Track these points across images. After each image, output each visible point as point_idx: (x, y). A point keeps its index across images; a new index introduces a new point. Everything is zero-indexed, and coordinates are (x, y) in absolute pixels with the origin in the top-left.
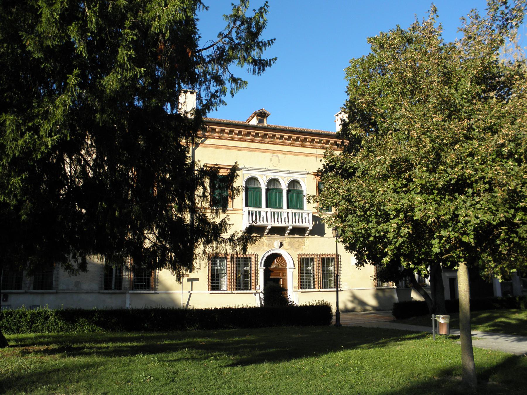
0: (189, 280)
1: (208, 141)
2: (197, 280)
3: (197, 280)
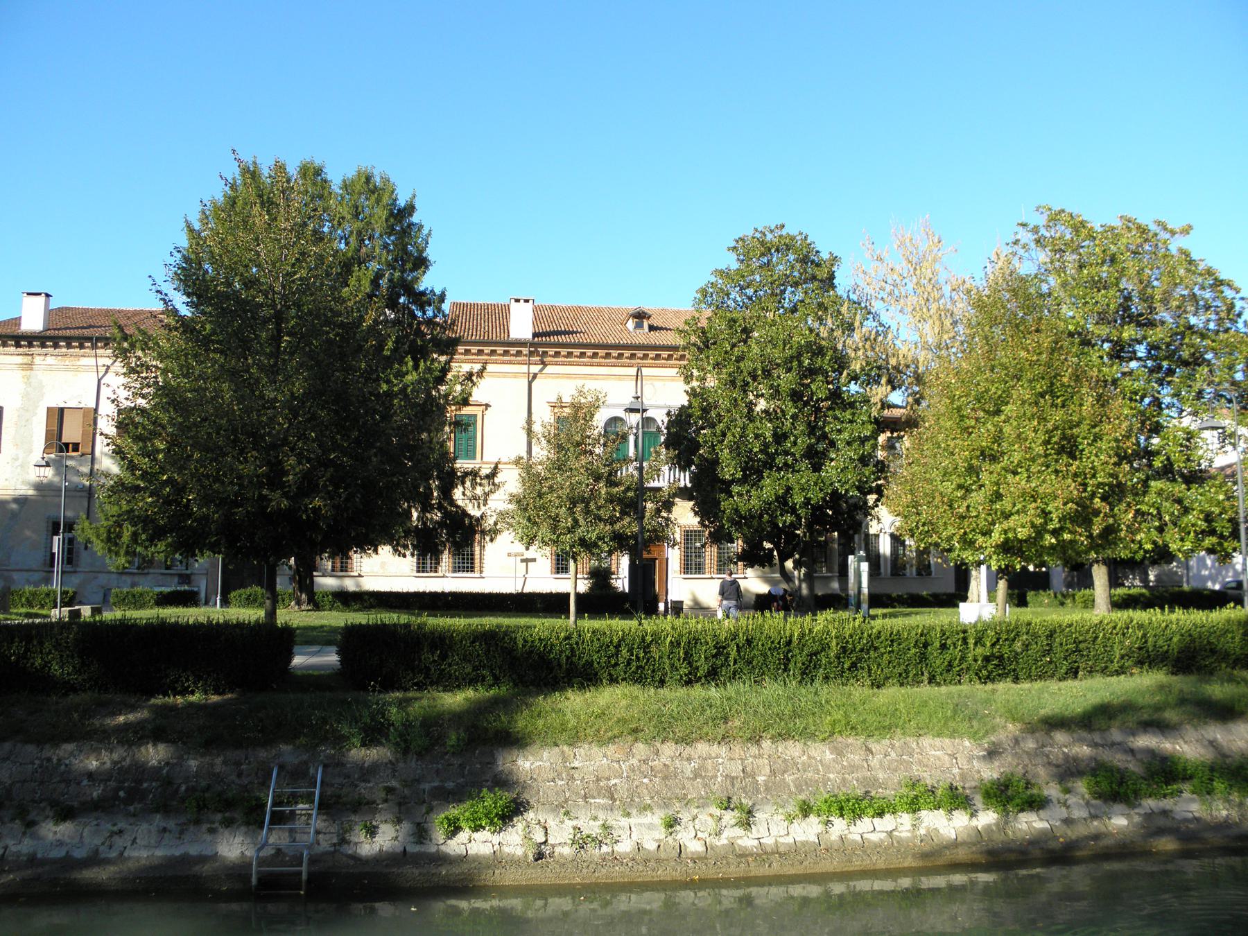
0: (523, 561)
1: (549, 369)
2: (534, 560)
3: (534, 560)
